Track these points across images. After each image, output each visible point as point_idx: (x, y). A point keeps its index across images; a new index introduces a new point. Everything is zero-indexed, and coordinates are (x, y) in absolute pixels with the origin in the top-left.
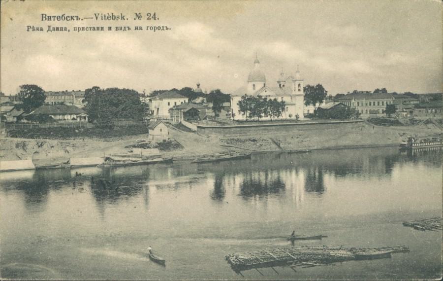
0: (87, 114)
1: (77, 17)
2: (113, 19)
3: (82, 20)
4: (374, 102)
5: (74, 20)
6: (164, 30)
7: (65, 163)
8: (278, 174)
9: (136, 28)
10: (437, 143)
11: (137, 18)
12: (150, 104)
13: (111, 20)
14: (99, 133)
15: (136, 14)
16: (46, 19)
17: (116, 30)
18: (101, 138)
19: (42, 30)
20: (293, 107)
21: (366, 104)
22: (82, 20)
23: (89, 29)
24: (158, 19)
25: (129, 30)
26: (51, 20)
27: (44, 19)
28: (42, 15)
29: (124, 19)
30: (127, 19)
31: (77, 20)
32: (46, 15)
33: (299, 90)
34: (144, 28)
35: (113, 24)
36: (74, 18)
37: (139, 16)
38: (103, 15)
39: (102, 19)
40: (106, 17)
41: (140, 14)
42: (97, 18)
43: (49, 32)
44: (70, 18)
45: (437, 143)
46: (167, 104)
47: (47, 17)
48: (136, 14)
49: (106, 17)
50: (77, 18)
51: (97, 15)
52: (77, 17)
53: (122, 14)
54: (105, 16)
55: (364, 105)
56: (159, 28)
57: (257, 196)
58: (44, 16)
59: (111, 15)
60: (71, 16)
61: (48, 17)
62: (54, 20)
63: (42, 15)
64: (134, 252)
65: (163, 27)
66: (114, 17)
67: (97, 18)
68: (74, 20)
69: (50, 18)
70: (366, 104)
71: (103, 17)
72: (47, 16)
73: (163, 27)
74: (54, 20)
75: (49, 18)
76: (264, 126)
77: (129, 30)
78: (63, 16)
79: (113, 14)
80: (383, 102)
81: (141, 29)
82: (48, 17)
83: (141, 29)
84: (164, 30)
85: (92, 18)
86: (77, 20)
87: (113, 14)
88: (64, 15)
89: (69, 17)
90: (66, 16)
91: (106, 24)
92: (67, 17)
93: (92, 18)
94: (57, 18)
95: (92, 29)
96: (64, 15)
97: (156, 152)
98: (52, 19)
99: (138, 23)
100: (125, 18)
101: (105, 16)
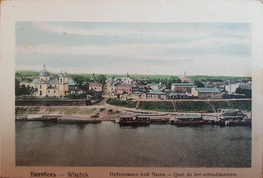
0: (72, 94)
1: (54, 174)
5: (52, 176)
7: (94, 117)
12: (104, 101)
14: (235, 139)
16: (34, 175)
23: (160, 175)
26: (37, 176)
27: (33, 175)
28: (32, 172)
31: (54, 176)
32: (34, 173)
36: (52, 175)
38: (74, 173)
42: (71, 176)
44: (50, 175)
46: (54, 92)
50: (54, 175)
52: (54, 174)
53: (86, 173)
58: (33, 173)
60: (50, 174)
61: (35, 174)
62: (39, 176)
63: (32, 172)
65: (161, 176)
67: (71, 176)
68: (52, 176)
69: (37, 174)
72: (215, 174)
74: (208, 176)
78: (45, 173)
79: (80, 173)
82: (35, 174)
87: (80, 173)
88: (46, 172)
89: (49, 174)
90: (47, 173)
92: (231, 174)
94: (41, 175)
95: (162, 175)
96: (46, 172)
98: (38, 175)
101: (75, 174)
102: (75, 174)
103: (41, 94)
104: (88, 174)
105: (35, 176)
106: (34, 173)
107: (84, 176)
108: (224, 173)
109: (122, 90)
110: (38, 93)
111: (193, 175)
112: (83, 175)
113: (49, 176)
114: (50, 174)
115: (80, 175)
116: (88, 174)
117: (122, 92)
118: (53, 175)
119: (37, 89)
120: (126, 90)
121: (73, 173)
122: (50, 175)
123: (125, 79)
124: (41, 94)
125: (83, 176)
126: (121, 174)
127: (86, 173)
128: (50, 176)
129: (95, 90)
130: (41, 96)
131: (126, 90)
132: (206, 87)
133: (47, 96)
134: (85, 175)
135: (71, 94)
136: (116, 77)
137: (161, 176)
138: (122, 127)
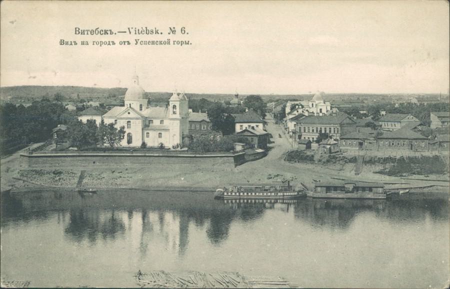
1: (111, 30)
2: (146, 33)
4: (325, 128)
5: (107, 34)
6: (110, 44)
9: (83, 43)
10: (269, 194)
11: (171, 33)
13: (145, 35)
15: (170, 28)
16: (79, 33)
17: (61, 44)
20: (167, 133)
21: (313, 131)
22: (115, 34)
25: (113, 44)
27: (77, 32)
29: (158, 33)
31: (111, 34)
32: (79, 29)
34: (117, 42)
37: (173, 31)
41: (174, 28)
45: (269, 194)
47: (80, 31)
48: (170, 28)
49: (140, 31)
51: (130, 29)
52: (111, 30)
53: (156, 28)
54: (139, 30)
55: (311, 131)
57: (61, 214)
58: (77, 29)
62: (124, 44)
64: (371, 161)
66: (148, 32)
68: (107, 34)
70: (313, 131)
73: (109, 42)
75: (83, 33)
76: (85, 156)
77: (113, 44)
79: (146, 28)
80: (330, 128)
84: (110, 44)
85: (125, 32)
86: (111, 34)
89: (103, 31)
93: (125, 32)
94: (91, 32)
98: (86, 33)
99: (172, 37)
103: (129, 142)
105: (82, 34)
109: (317, 130)
110: (124, 140)
111: (79, 43)
113: (103, 34)
115: (145, 31)
117: (315, 136)
118: (109, 32)
119: (122, 131)
120: (330, 131)
123: (313, 104)
124: (129, 142)
131: (330, 131)
132: (193, 271)
136: (291, 100)
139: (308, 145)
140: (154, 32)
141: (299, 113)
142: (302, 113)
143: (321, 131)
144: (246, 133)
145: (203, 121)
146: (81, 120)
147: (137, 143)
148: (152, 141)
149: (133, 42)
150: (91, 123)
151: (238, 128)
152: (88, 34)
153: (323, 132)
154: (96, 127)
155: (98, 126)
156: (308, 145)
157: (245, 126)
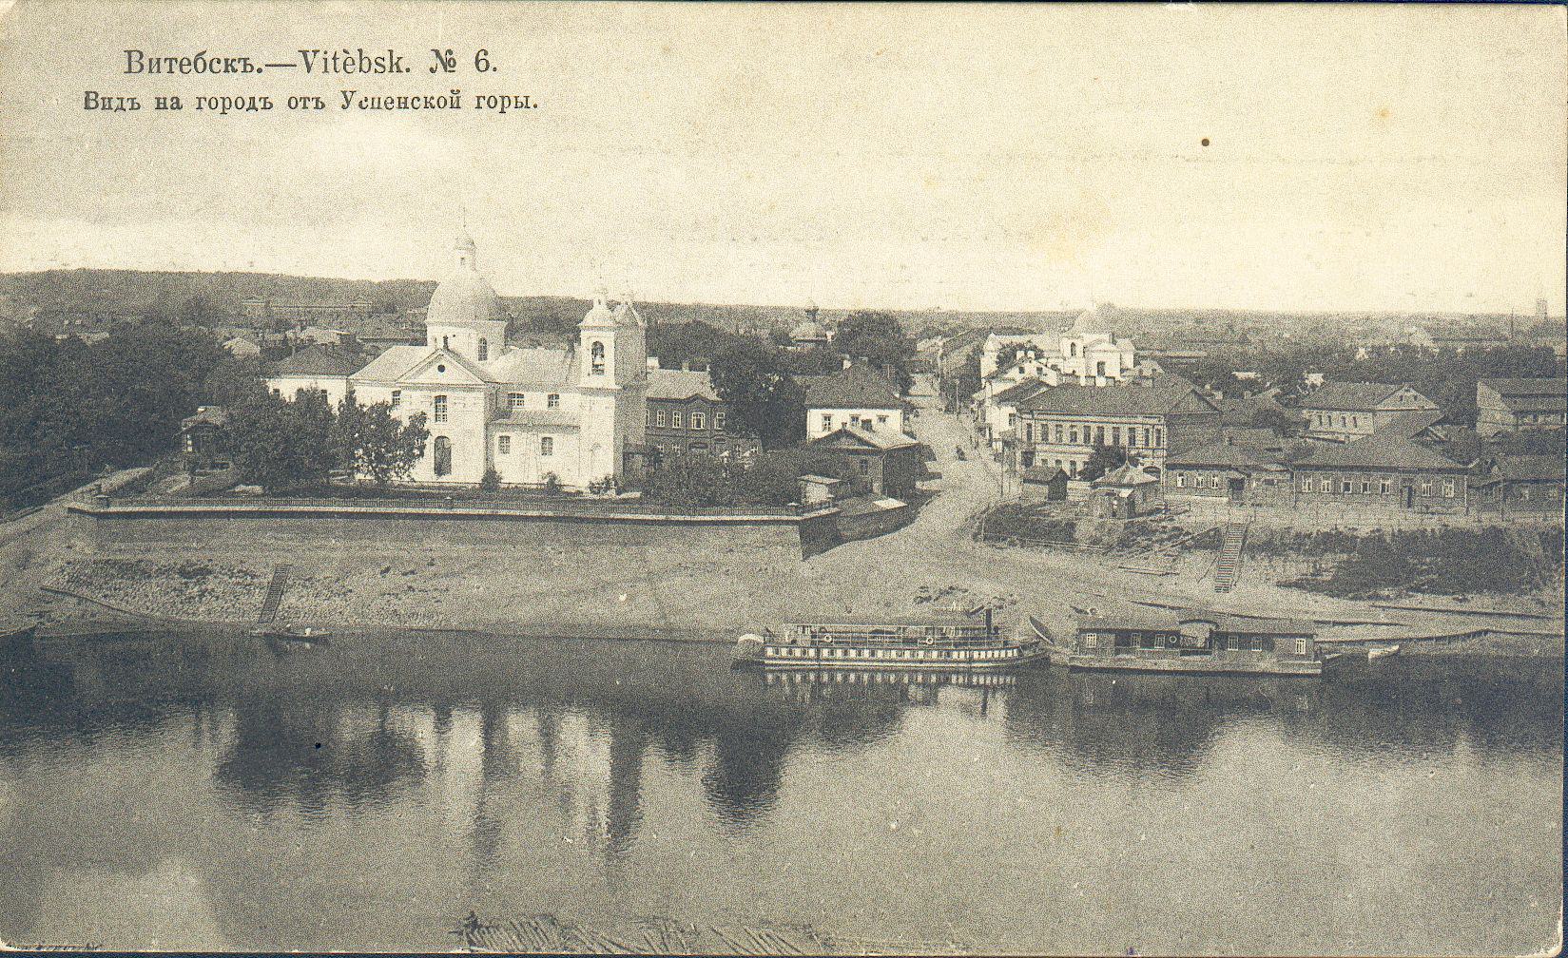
3: (259, 71)
8: (383, 715)
9: (161, 104)
18: (1203, 737)
19: (320, 105)
20: (571, 439)
23: (301, 104)
24: (432, 71)
26: (159, 71)
27: (136, 67)
29: (399, 71)
30: (408, 70)
33: (597, 369)
34: (188, 102)
35: (366, 85)
38: (330, 56)
39: (326, 71)
40: (340, 64)
41: (450, 52)
43: (253, 111)
47: (145, 61)
49: (340, 64)
50: (245, 65)
52: (317, 99)
56: (238, 104)
58: (135, 56)
59: (356, 56)
60: (226, 60)
61: (103, 99)
65: (305, 107)
71: (331, 62)
79: (360, 51)
81: (177, 105)
82: (151, 60)
83: (177, 105)
86: (245, 71)
89: (219, 62)
90: (207, 57)
91: (327, 85)
94: (181, 65)
95: (115, 104)
97: (160, 556)
98: (164, 66)
100: (403, 65)
102: (334, 59)
103: (441, 468)
104: (399, 58)
106: (141, 57)
107: (379, 61)
108: (233, 57)
109: (1087, 437)
112: (374, 66)
114: (226, 60)
116: (399, 58)
117: (1082, 456)
118: (240, 67)
120: (1132, 440)
121: (320, 55)
122: (227, 65)
125: (376, 71)
126: (499, 100)
127: (391, 51)
128: (226, 71)
129: (861, 441)
130: (444, 479)
133: (491, 478)
134: (387, 64)
135: (876, 502)
137: (305, 107)
138: (1499, 766)
139: (1057, 483)
140: (388, 69)
141: (1026, 375)
142: (1035, 374)
143: (1100, 438)
144: (845, 444)
145: (695, 397)
146: (277, 391)
147: (466, 471)
148: (520, 467)
149: (333, 98)
150: (313, 401)
151: (816, 424)
152: (171, 72)
153: (1108, 441)
154: (328, 413)
155: (335, 411)
156: (1057, 483)
157: (840, 417)
